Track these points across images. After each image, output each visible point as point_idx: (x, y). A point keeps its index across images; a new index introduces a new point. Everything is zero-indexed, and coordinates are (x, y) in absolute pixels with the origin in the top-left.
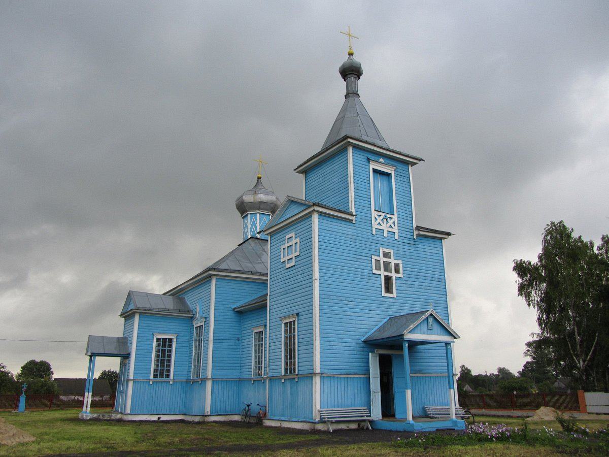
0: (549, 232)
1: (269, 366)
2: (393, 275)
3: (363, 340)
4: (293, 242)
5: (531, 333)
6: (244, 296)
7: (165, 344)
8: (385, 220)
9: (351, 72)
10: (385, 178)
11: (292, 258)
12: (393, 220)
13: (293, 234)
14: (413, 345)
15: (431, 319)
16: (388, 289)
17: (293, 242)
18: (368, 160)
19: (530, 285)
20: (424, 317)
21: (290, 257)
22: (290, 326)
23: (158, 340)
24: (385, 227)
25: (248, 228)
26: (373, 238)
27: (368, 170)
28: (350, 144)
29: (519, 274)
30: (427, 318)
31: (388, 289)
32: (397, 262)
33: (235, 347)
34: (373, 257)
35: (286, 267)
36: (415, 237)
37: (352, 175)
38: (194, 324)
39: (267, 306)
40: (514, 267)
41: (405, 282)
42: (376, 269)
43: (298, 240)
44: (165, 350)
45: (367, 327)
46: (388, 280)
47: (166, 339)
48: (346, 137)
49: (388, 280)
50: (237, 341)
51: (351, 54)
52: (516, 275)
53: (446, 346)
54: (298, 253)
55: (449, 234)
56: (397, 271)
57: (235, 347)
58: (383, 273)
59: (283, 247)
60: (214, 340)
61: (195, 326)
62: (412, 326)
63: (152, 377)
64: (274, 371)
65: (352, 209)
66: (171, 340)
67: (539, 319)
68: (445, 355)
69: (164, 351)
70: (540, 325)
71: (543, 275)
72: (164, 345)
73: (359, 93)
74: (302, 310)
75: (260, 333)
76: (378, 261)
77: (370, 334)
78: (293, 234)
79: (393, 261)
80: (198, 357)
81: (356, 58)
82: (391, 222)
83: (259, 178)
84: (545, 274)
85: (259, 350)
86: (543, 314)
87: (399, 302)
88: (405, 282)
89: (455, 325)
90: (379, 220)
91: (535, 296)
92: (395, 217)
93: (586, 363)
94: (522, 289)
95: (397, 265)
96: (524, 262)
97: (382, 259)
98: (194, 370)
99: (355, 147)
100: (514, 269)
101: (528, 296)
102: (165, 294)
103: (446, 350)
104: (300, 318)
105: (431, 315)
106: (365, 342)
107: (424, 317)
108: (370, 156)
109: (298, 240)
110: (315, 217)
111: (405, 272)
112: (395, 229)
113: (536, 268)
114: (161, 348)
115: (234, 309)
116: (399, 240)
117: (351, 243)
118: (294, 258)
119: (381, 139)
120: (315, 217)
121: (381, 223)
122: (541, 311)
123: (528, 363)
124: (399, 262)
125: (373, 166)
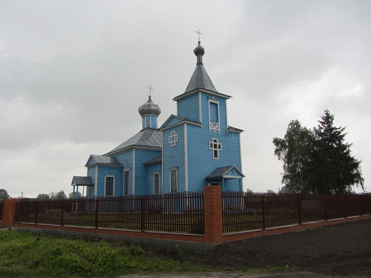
0: (291, 124)
1: (164, 189)
2: (218, 149)
3: (205, 178)
4: (175, 135)
5: (280, 173)
6: (147, 159)
7: (109, 180)
8: (215, 126)
9: (199, 52)
10: (215, 105)
11: (174, 143)
12: (218, 125)
13: (175, 132)
14: (226, 179)
15: (234, 169)
16: (216, 156)
17: (175, 135)
18: (208, 98)
19: (281, 150)
20: (231, 168)
21: (173, 142)
22: (173, 173)
23: (107, 178)
24: (214, 128)
25: (145, 123)
26: (209, 133)
27: (207, 104)
28: (200, 91)
29: (275, 145)
30: (232, 169)
31: (216, 156)
32: (219, 144)
33: (144, 181)
34: (209, 142)
35: (171, 146)
36: (227, 133)
37: (201, 105)
38: (124, 170)
39: (162, 162)
40: (273, 141)
41: (223, 153)
42: (211, 147)
43: (177, 135)
44: (110, 182)
45: (207, 172)
46: (216, 152)
47: (110, 177)
48: (198, 89)
49: (216, 152)
50: (145, 178)
51: (199, 43)
52: (274, 145)
53: (240, 180)
54: (177, 141)
55: (242, 131)
56: (219, 148)
57: (144, 181)
58: (213, 149)
59: (169, 137)
60: (135, 177)
61: (124, 171)
62: (226, 172)
63: (105, 195)
64: (166, 191)
65: (201, 121)
66: (113, 178)
67: (284, 166)
68: (239, 184)
69: (110, 183)
70: (285, 169)
71: (287, 145)
72: (110, 180)
73: (203, 63)
74: (180, 165)
75: (157, 175)
76: (211, 144)
77: (208, 175)
78: (175, 132)
79: (218, 144)
80: (127, 186)
81: (202, 45)
82: (217, 126)
83: (150, 97)
84: (288, 144)
85: (157, 181)
86: (286, 164)
87: (220, 162)
88: (223, 153)
89: (243, 172)
90: (212, 125)
91: (283, 155)
92: (219, 124)
93: (304, 187)
94: (277, 152)
95: (219, 146)
96: (278, 138)
97: (213, 143)
98: (124, 191)
99: (202, 92)
100: (273, 142)
101: (279, 154)
102: (104, 155)
103: (240, 182)
104: (178, 169)
105: (234, 167)
106: (206, 179)
107: (231, 168)
108: (208, 96)
109: (177, 135)
110: (185, 126)
111: (223, 148)
112: (219, 129)
113: (284, 141)
114: (111, 182)
115: (143, 164)
116: (221, 134)
117: (200, 136)
118: (175, 143)
119: (213, 86)
120: (185, 126)
121: (213, 127)
122: (285, 162)
123: (283, 187)
124: (220, 144)
125: (210, 101)
